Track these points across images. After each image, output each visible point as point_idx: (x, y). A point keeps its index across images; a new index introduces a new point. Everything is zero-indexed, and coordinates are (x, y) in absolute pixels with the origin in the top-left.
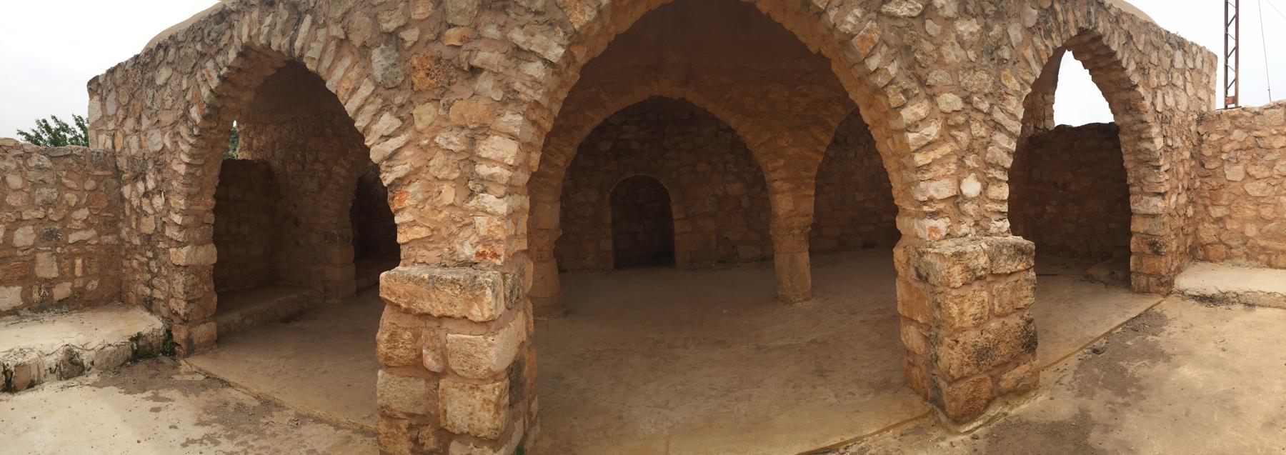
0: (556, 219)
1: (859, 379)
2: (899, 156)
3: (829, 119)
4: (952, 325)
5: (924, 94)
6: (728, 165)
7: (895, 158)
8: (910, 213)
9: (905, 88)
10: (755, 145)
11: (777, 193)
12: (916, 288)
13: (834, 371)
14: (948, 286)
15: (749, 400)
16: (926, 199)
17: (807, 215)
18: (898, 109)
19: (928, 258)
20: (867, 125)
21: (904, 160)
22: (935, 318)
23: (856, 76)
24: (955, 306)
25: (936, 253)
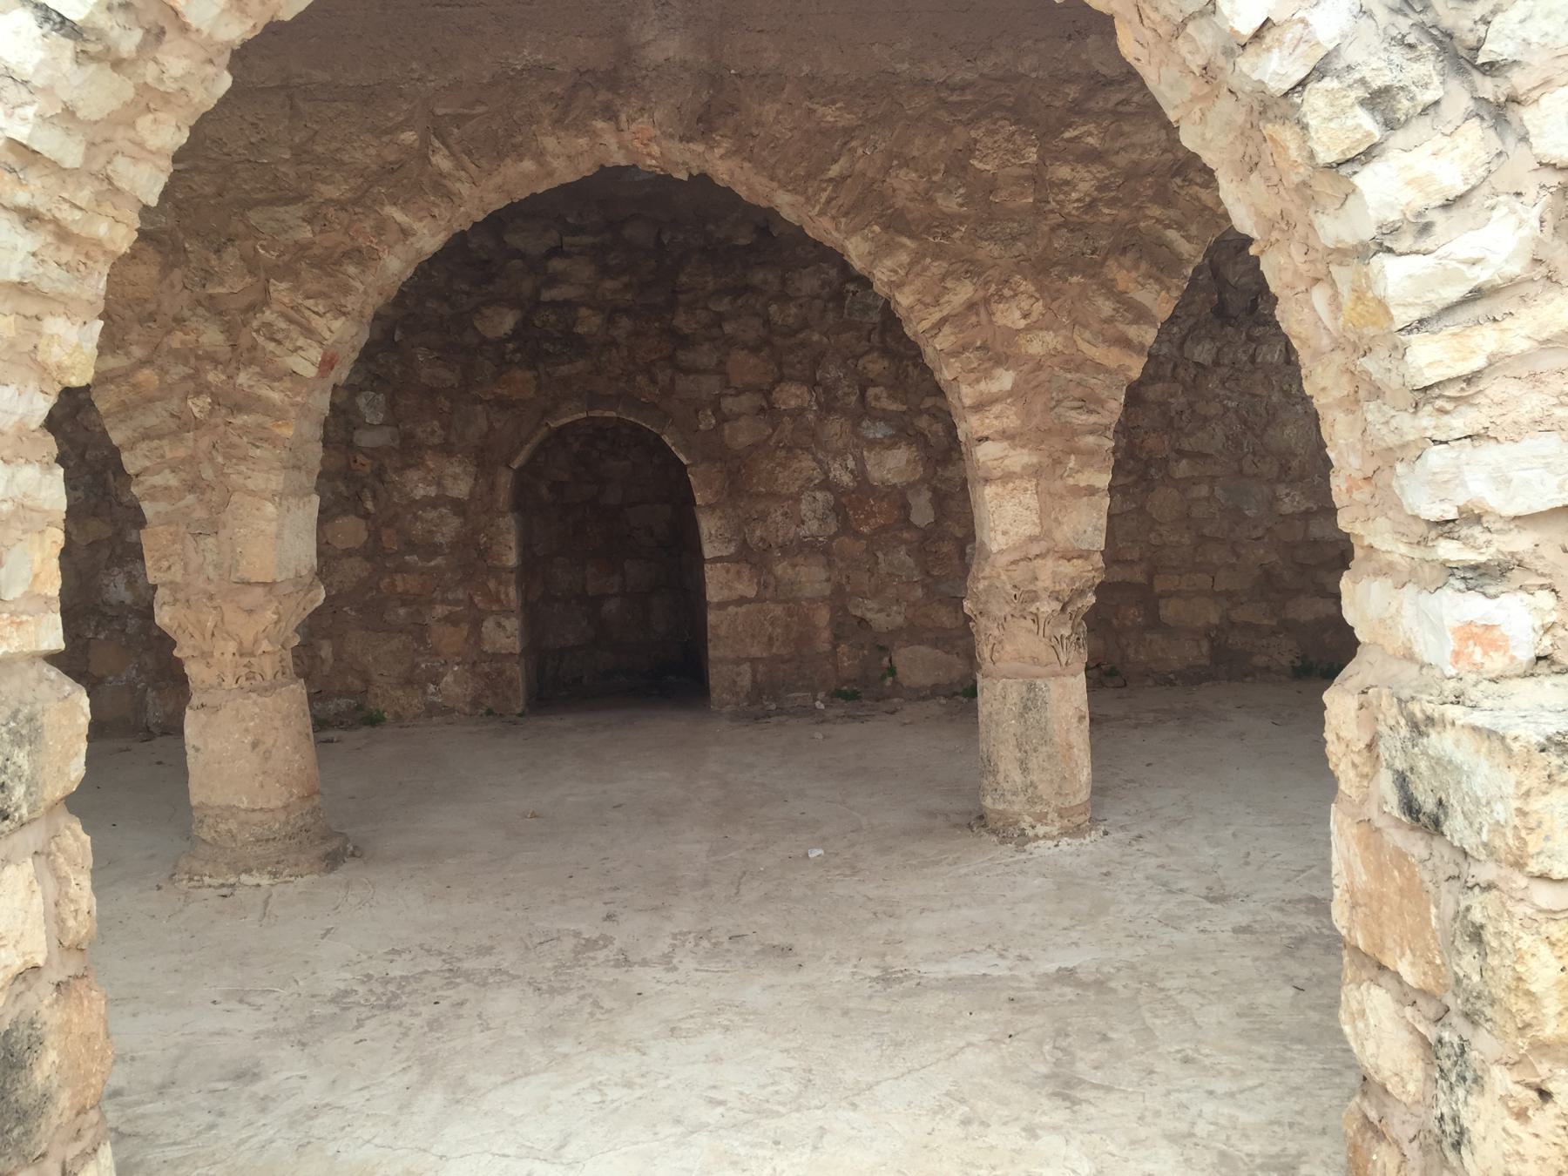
0: (302, 551)
1: (1192, 1135)
2: (1355, 348)
3: (1172, 234)
4: (1527, 1026)
5: (1465, 102)
6: (871, 392)
7: (1339, 358)
8: (1391, 565)
9: (1377, 83)
10: (926, 325)
11: (987, 481)
12: (1397, 849)
13: (1109, 1089)
14: (1519, 865)
15: (815, 1148)
16: (1452, 514)
17: (1084, 555)
18: (1344, 170)
19: (1440, 742)
20: (1249, 241)
21: (1368, 364)
22: (1458, 981)
23: (1196, 63)
24: (1544, 950)
25: (1475, 729)
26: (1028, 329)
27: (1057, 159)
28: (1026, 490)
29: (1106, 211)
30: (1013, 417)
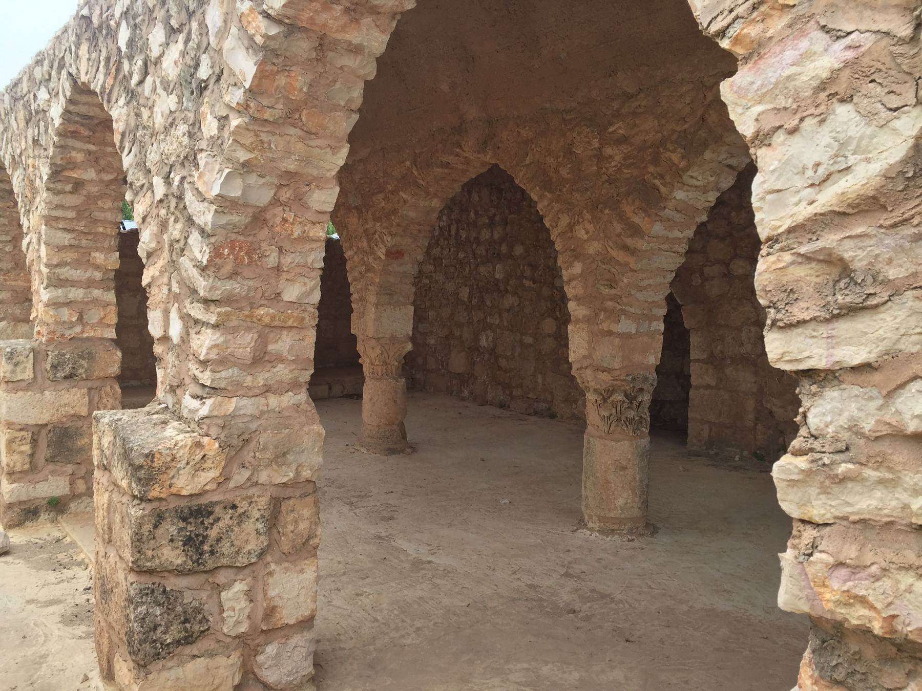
26: (588, 240)
27: (606, 144)
28: (583, 329)
29: (626, 171)
30: (581, 288)
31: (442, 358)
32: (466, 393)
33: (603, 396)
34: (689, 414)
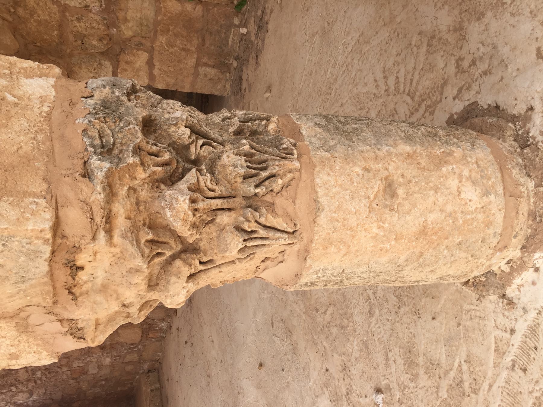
31: (125, 349)
32: (163, 325)
33: (174, 257)
34: (186, 91)
